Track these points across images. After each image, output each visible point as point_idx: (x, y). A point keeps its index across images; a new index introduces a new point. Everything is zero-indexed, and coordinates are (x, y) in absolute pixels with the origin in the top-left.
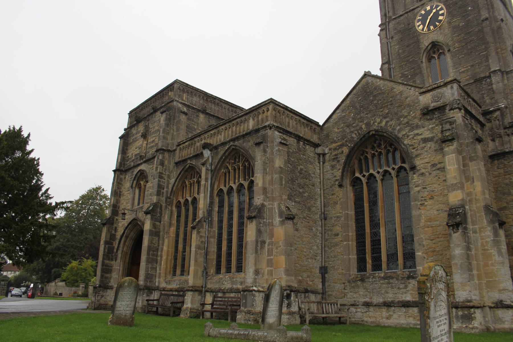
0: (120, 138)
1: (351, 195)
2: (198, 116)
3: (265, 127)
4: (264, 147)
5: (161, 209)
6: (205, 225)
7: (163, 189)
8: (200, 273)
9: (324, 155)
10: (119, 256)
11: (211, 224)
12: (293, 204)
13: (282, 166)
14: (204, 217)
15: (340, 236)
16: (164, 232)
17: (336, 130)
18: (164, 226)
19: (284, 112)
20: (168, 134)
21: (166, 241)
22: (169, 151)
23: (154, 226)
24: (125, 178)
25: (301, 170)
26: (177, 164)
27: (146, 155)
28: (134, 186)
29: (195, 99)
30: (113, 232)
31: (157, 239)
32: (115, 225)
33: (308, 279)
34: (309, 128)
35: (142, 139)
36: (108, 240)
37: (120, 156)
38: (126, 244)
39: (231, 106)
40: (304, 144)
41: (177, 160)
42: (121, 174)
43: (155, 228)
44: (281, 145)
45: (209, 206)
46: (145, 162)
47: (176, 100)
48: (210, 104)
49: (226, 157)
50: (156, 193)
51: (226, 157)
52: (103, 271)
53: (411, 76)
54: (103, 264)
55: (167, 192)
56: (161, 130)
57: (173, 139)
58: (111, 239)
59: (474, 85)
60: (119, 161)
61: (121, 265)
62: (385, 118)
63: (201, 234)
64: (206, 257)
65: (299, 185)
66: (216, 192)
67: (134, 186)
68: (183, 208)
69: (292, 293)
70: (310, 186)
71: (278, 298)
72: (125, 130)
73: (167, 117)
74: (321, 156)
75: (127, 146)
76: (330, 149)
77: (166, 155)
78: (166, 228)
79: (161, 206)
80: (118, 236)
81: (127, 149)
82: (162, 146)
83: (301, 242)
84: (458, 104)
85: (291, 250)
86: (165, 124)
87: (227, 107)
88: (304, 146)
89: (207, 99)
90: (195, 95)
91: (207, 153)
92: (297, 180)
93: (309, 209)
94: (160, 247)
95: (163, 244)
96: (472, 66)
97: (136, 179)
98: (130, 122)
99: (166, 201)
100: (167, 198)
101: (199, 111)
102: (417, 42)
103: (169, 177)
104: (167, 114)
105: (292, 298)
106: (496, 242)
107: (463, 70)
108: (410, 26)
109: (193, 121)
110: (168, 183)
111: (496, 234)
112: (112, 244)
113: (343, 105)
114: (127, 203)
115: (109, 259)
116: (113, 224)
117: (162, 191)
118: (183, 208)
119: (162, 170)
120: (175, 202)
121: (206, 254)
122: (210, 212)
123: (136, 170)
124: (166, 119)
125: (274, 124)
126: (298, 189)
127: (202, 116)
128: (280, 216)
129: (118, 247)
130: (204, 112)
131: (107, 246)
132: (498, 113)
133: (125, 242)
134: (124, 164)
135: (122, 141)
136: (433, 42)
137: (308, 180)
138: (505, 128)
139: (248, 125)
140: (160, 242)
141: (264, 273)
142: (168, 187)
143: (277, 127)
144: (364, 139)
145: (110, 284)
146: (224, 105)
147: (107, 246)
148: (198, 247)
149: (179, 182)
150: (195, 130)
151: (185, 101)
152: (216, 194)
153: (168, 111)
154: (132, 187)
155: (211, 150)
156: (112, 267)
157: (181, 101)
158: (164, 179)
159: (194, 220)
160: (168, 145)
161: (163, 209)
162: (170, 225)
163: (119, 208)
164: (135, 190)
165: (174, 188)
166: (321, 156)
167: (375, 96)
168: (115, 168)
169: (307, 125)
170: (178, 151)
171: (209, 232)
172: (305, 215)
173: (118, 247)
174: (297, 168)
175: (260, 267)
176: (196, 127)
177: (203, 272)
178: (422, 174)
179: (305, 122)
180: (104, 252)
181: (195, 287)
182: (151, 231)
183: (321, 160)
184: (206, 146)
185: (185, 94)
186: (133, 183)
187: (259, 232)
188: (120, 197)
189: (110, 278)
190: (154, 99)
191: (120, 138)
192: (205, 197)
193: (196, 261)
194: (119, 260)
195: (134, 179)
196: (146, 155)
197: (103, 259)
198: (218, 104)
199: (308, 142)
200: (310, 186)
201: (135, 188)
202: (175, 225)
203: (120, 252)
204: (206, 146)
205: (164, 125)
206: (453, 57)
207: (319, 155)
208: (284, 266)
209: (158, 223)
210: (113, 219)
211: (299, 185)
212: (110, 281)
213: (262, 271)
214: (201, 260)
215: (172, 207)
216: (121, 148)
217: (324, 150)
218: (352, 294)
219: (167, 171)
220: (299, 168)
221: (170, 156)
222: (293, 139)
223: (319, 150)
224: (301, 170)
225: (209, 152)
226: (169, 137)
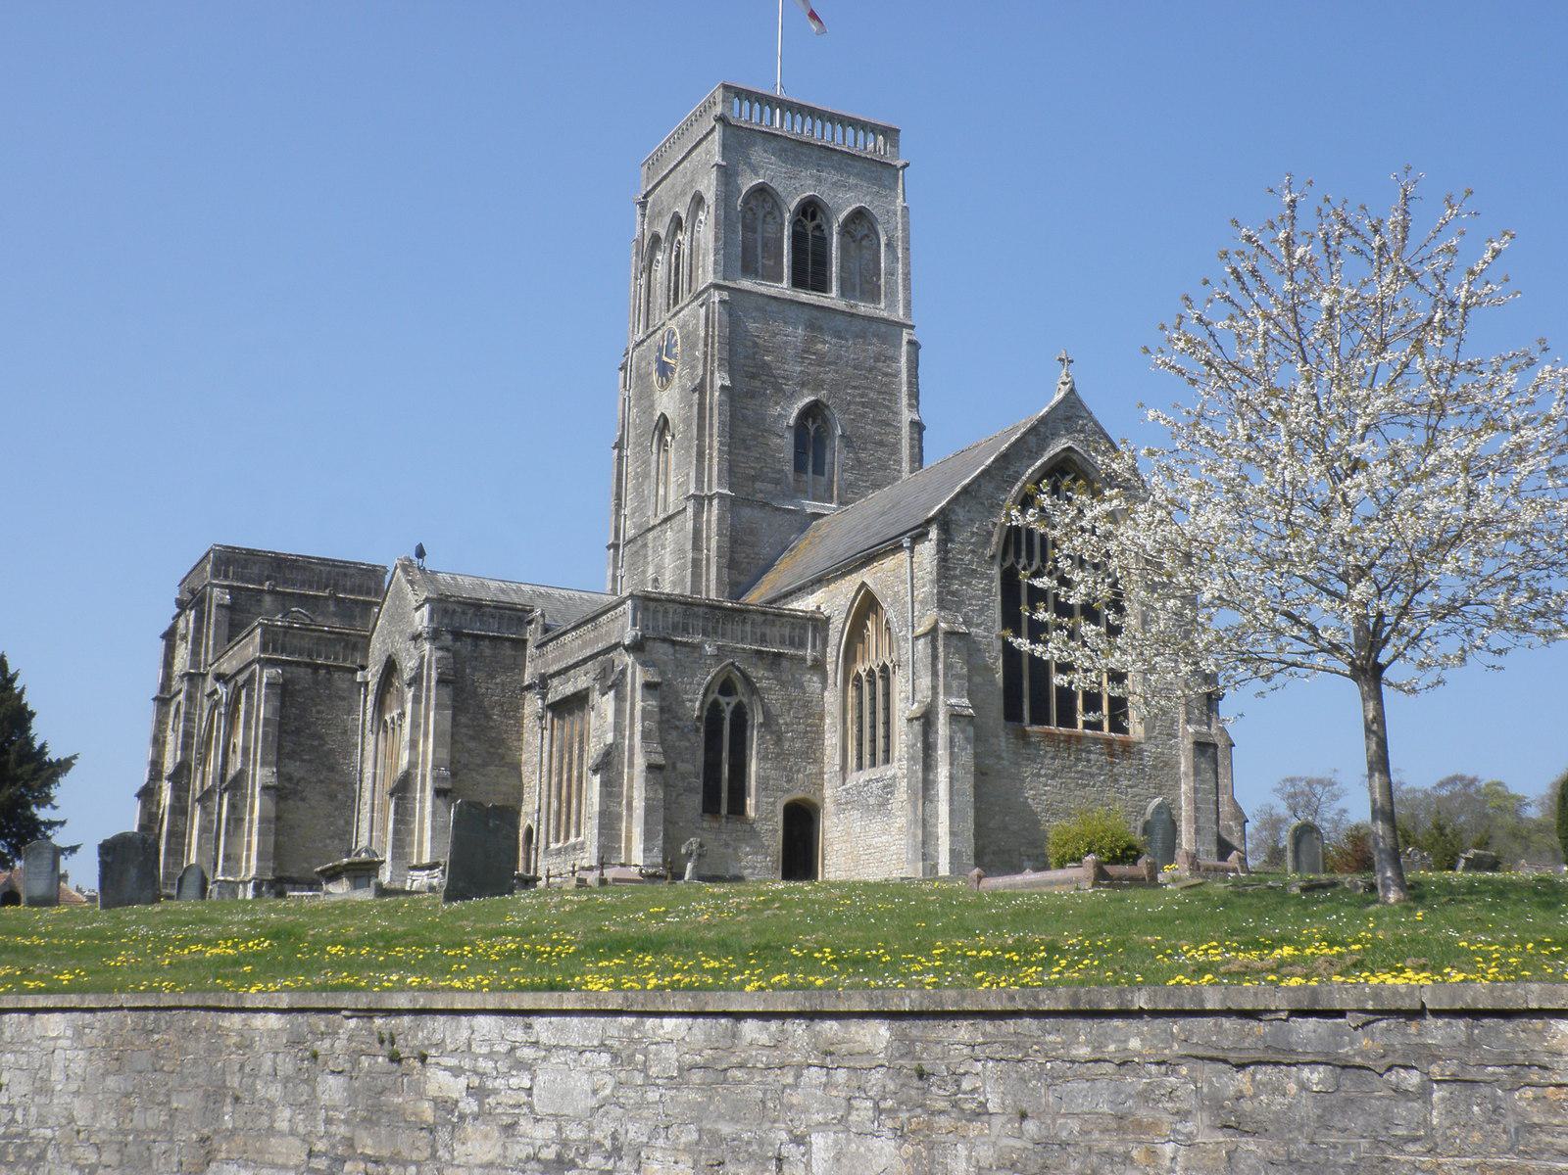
2: (259, 601)
14: (214, 785)
40: (329, 672)
68: (880, 683)
118: (880, 683)
179: (333, 636)
187: (233, 807)
209: (182, 794)
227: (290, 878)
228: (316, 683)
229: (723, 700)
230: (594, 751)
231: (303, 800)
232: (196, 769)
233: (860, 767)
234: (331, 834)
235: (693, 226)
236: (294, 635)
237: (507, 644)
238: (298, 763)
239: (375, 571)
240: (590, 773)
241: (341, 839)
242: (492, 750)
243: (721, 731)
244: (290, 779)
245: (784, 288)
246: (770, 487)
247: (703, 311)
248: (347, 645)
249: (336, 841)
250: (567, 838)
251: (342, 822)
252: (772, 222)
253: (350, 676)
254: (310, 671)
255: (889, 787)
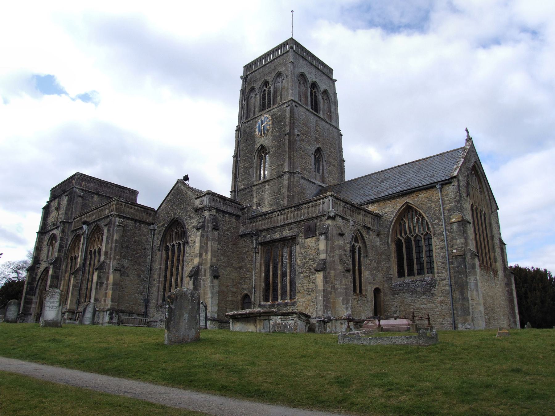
0: (43, 209)
1: (164, 256)
2: (93, 197)
3: (111, 215)
4: (108, 227)
5: (61, 262)
6: (80, 273)
7: (63, 248)
8: (74, 301)
9: (155, 230)
10: (37, 292)
11: (84, 272)
12: (127, 261)
13: (118, 239)
14: (80, 267)
15: (155, 281)
16: (61, 276)
17: (162, 215)
18: (62, 272)
19: (125, 205)
20: (69, 211)
21: (62, 282)
22: (69, 222)
23: (55, 272)
24: (45, 238)
25: (135, 240)
26: (72, 231)
27: (57, 223)
28: (49, 244)
29: (92, 185)
30: (34, 276)
31: (57, 280)
32: (36, 271)
33: (134, 306)
34: (146, 213)
35: (56, 211)
36: (30, 281)
37: (42, 222)
38: (42, 284)
39: (121, 188)
40: (140, 224)
41: (72, 229)
42: (42, 235)
43: (56, 274)
44: (119, 227)
45: (84, 261)
46: (56, 228)
47: (76, 187)
48: (103, 188)
49: (95, 231)
50: (57, 250)
51: (95, 231)
52: (25, 303)
53: (248, 168)
54: (26, 298)
55: (65, 250)
56: (64, 208)
57: (72, 214)
58: (32, 281)
59: (277, 180)
60: (41, 226)
61: (38, 299)
62: (182, 211)
63: (77, 278)
64: (79, 292)
65: (133, 250)
66: (89, 252)
67: (49, 244)
69: (114, 312)
70: (142, 250)
71: (92, 312)
72: (48, 202)
73: (68, 199)
74: (153, 231)
75: (48, 215)
76: (158, 227)
77: (67, 225)
78: (63, 274)
79: (61, 259)
80: (38, 277)
81: (47, 217)
82: (64, 219)
83: (131, 284)
84: (208, 208)
85: (117, 288)
86: (67, 204)
87: (117, 189)
88: (140, 225)
89: (101, 184)
90: (92, 182)
91: (85, 227)
92: (132, 246)
93: (139, 264)
94: (59, 286)
95: (60, 284)
96: (278, 166)
97: (51, 239)
98: (51, 198)
99: (64, 255)
100: (65, 254)
101: (94, 193)
102: (254, 143)
103: (67, 240)
104: (68, 197)
105: (114, 315)
106: (212, 286)
107: (274, 168)
108: (252, 130)
109: (89, 201)
110: (67, 244)
111: (212, 282)
112: (33, 284)
113: (167, 199)
114: (44, 256)
115: (29, 295)
116: (34, 270)
117: (62, 249)
119: (63, 235)
120: (70, 256)
121: (80, 290)
122: (84, 265)
123: (51, 233)
124: (68, 201)
125: (116, 213)
126: (131, 252)
127: (96, 197)
128: (113, 269)
129: (37, 286)
130: (97, 194)
131: (29, 286)
132: (247, 209)
133: (41, 283)
134: (45, 228)
135: (44, 211)
136: (262, 145)
137: (140, 246)
138: (248, 219)
139: (105, 212)
140: (59, 283)
141: (101, 301)
142: (66, 247)
143: (118, 215)
144: (172, 223)
145: (30, 312)
146: (115, 188)
147: (29, 286)
148: (74, 286)
149: (73, 244)
150: (90, 207)
151: (83, 187)
152: (89, 253)
153: (69, 195)
154: (47, 245)
155: (88, 225)
156: (32, 300)
157: (81, 188)
158: (64, 242)
159: (75, 268)
160: (69, 218)
161: (62, 260)
162: (66, 272)
163: (39, 259)
164: (49, 247)
165: (69, 248)
166: (153, 231)
167: (180, 196)
168: (38, 231)
169: (144, 211)
170: (73, 223)
171: (83, 276)
172: (135, 268)
173: (37, 286)
174: (133, 239)
175: (98, 297)
176: (90, 205)
177: (77, 301)
178: (190, 246)
179: (142, 209)
180: (27, 289)
181: (70, 309)
182: (52, 275)
183: (153, 234)
184: (85, 223)
185: (83, 182)
186: (48, 242)
187: (99, 277)
188: (40, 251)
189: (31, 308)
190: (65, 183)
191: (43, 209)
192: (82, 255)
193: (72, 294)
194: (37, 296)
195: (49, 240)
196: (57, 223)
197: (26, 294)
198: (110, 187)
199: (142, 222)
200: (142, 250)
201: (50, 246)
202: (69, 272)
203: (38, 290)
204: (85, 223)
205: (66, 204)
206: (270, 157)
207: (152, 230)
208: (111, 297)
209: (57, 270)
210: (35, 266)
211: (133, 250)
212: (30, 310)
213: (100, 299)
214: (76, 293)
215: (68, 260)
216: (43, 216)
217: (154, 227)
218: (156, 315)
219: (66, 236)
220: (134, 239)
221: (69, 226)
222: (131, 221)
223: (151, 227)
224: (135, 240)
225: (87, 227)
226: (70, 213)
227: (122, 310)
228: (135, 228)
229: (356, 244)
230: (188, 269)
231: (128, 276)
232: (64, 260)
233: (401, 274)
234: (137, 292)
235: (275, 83)
236: (128, 207)
237: (234, 217)
238: (127, 261)
239: (135, 192)
240: (188, 278)
241: (141, 294)
242: (229, 261)
243: (403, 259)
244: (123, 267)
245: (309, 108)
246: (308, 173)
247: (288, 109)
248: (147, 213)
249: (140, 295)
250: (275, 299)
251: (142, 287)
252: (303, 86)
253: (148, 226)
254: (133, 222)
255: (433, 284)
